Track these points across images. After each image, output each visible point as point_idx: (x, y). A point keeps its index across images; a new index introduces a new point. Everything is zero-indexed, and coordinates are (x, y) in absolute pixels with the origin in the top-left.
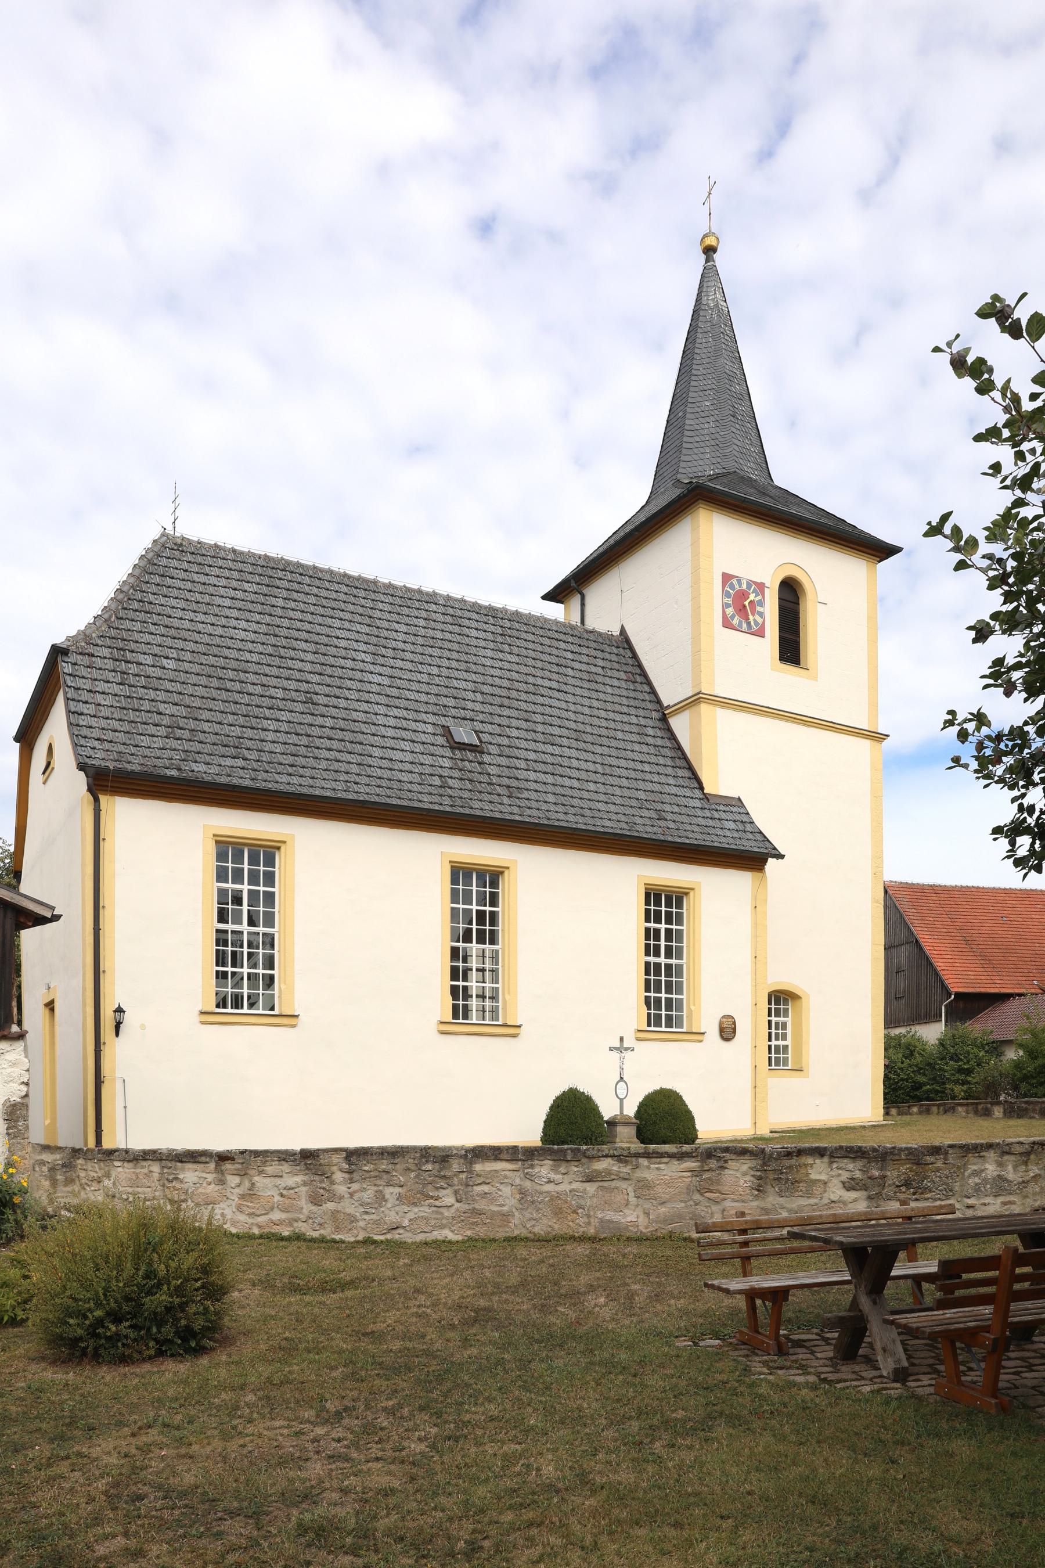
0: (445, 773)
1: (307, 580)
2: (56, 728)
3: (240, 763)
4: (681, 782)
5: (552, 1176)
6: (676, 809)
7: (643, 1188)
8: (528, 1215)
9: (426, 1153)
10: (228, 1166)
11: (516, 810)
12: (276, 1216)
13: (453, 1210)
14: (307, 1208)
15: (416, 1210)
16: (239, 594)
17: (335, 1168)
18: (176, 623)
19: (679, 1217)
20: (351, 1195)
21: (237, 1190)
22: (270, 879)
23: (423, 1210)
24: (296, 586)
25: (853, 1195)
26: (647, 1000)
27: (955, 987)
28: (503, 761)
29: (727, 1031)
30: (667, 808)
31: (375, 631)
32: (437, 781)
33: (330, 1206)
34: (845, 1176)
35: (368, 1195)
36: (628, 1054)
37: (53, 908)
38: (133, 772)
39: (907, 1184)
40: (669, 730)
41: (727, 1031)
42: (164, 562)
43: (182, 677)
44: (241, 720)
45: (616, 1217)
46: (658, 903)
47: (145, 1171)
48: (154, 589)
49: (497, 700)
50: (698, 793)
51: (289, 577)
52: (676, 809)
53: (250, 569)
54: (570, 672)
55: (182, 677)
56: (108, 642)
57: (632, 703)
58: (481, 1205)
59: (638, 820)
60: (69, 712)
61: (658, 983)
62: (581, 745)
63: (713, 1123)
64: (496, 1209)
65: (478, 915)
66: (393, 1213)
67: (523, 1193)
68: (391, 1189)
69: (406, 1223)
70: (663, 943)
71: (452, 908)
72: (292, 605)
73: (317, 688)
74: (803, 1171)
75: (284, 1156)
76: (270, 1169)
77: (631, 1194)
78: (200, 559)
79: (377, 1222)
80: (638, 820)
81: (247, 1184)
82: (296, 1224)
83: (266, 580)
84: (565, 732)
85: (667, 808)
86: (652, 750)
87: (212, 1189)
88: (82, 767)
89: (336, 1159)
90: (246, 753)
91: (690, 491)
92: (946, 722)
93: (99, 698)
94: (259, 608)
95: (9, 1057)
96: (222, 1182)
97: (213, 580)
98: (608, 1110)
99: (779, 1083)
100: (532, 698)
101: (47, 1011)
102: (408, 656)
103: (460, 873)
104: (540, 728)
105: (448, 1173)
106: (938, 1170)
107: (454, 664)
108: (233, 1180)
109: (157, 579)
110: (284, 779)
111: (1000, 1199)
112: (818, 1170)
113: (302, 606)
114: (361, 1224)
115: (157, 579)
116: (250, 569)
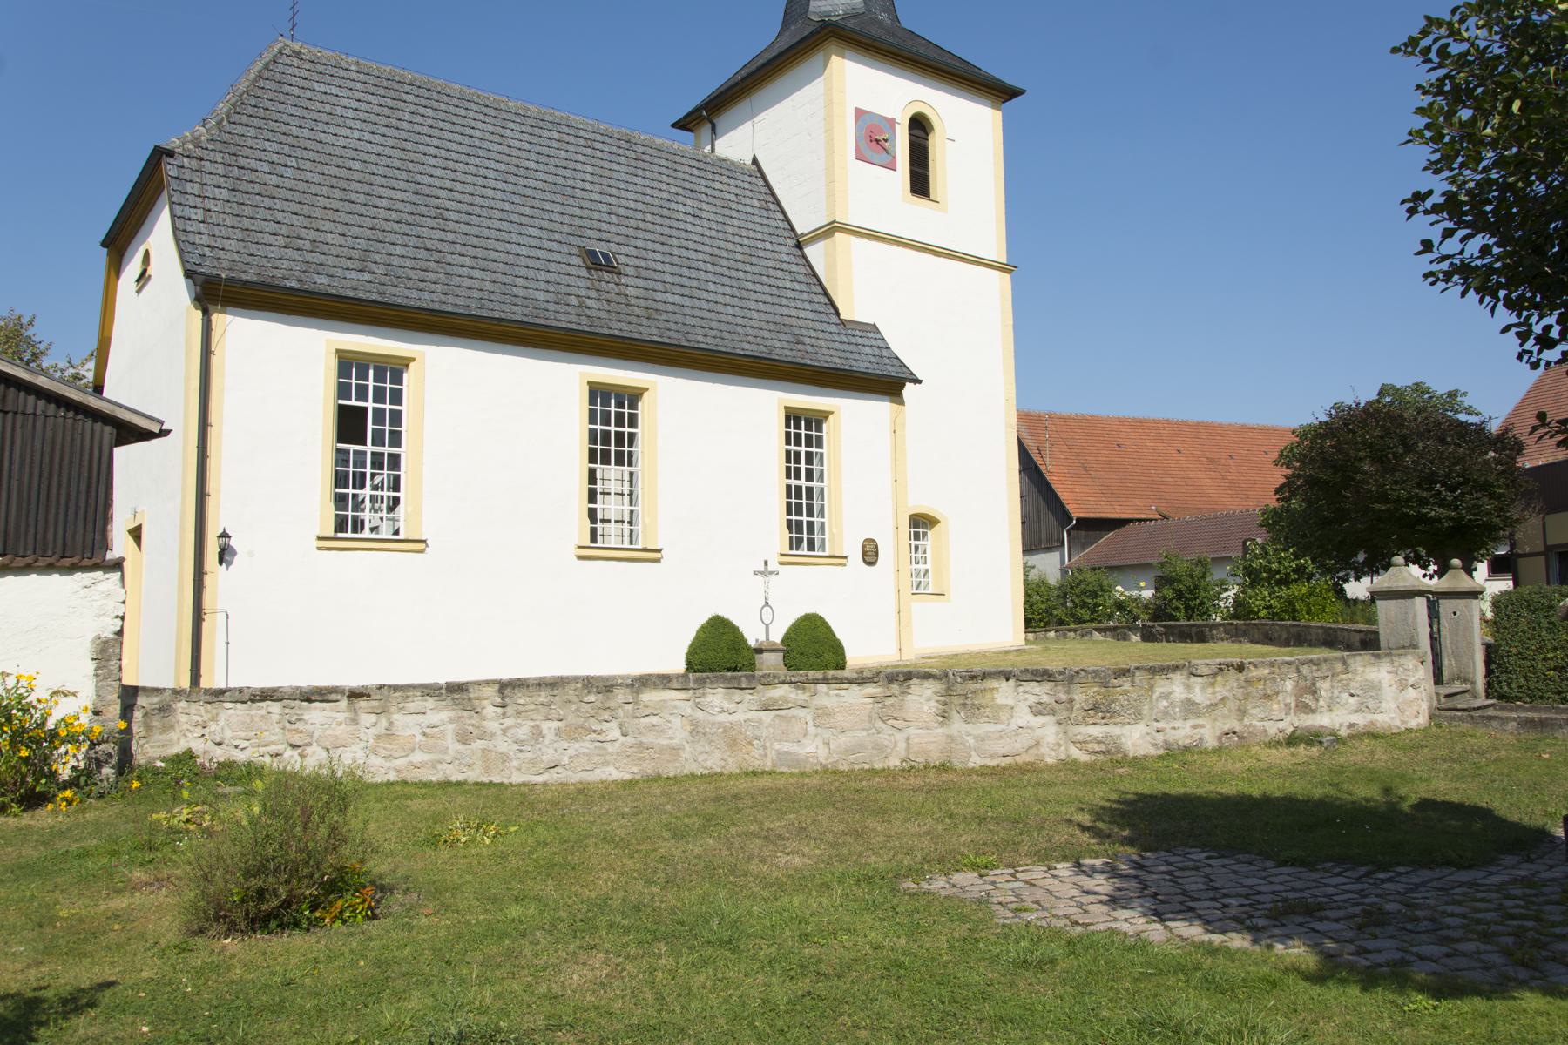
0: (582, 292)
1: (435, 96)
2: (160, 238)
3: (367, 276)
4: (817, 307)
5: (726, 705)
6: (813, 334)
7: (823, 714)
8: (699, 749)
9: (589, 683)
10: (362, 703)
11: (655, 331)
12: (418, 757)
13: (617, 744)
14: (453, 746)
15: (577, 745)
16: (363, 106)
17: (485, 703)
18: (295, 131)
19: (860, 747)
20: (504, 731)
21: (373, 731)
22: (397, 397)
23: (585, 745)
24: (423, 101)
25: (1041, 719)
26: (789, 523)
27: (1077, 512)
28: (641, 282)
29: (870, 554)
30: (804, 332)
31: (506, 150)
32: (574, 301)
33: (479, 744)
34: (1032, 700)
35: (523, 731)
36: (773, 578)
37: (162, 423)
38: (248, 282)
39: (1095, 707)
40: (804, 257)
41: (870, 554)
42: (280, 68)
43: (302, 186)
44: (368, 233)
45: (794, 748)
46: (798, 426)
47: (263, 712)
48: (271, 95)
49: (632, 223)
50: (834, 318)
51: (416, 91)
52: (813, 334)
53: (375, 81)
54: (703, 197)
55: (302, 186)
56: (219, 146)
57: (766, 229)
58: (648, 739)
59: (778, 344)
60: (173, 216)
61: (799, 506)
62: (718, 269)
63: (864, 646)
64: (665, 742)
65: (612, 433)
66: (551, 751)
67: (694, 724)
68: (549, 724)
69: (566, 760)
70: (803, 466)
71: (338, 451)
72: (419, 119)
73: (448, 204)
74: (988, 695)
75: (429, 690)
76: (411, 706)
77: (810, 723)
78: (320, 68)
79: (533, 762)
80: (778, 344)
81: (384, 722)
82: (439, 766)
83: (392, 94)
84: (701, 256)
85: (804, 332)
86: (788, 276)
87: (343, 731)
88: (189, 274)
89: (491, 692)
90: (374, 268)
91: (822, 28)
92: (1408, 211)
93: (209, 204)
94: (384, 121)
95: (101, 587)
96: (354, 721)
97: (334, 90)
98: (753, 635)
99: (921, 608)
100: (667, 221)
101: (131, 540)
102: (541, 176)
103: (598, 393)
104: (676, 251)
105: (612, 704)
106: (1126, 692)
107: (588, 186)
108: (367, 719)
109: (274, 86)
110: (415, 294)
111: (1190, 723)
112: (1004, 692)
113: (431, 122)
114: (515, 763)
115: (274, 86)
116: (375, 81)
